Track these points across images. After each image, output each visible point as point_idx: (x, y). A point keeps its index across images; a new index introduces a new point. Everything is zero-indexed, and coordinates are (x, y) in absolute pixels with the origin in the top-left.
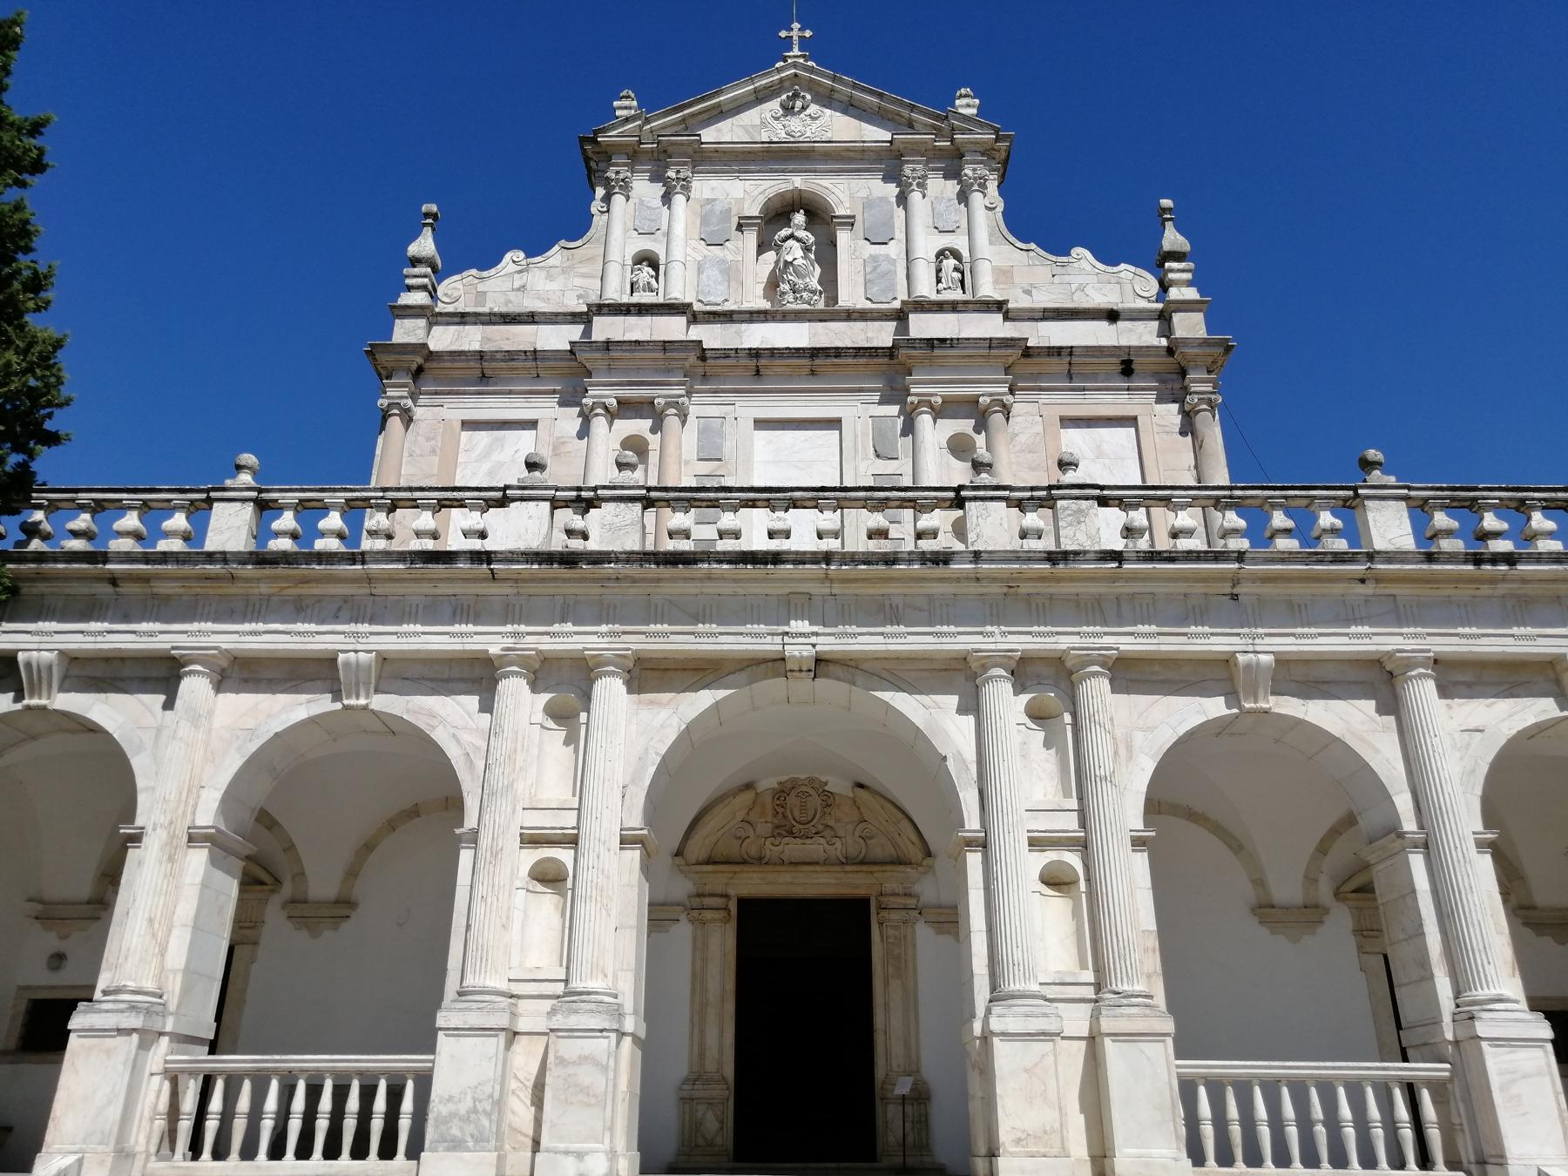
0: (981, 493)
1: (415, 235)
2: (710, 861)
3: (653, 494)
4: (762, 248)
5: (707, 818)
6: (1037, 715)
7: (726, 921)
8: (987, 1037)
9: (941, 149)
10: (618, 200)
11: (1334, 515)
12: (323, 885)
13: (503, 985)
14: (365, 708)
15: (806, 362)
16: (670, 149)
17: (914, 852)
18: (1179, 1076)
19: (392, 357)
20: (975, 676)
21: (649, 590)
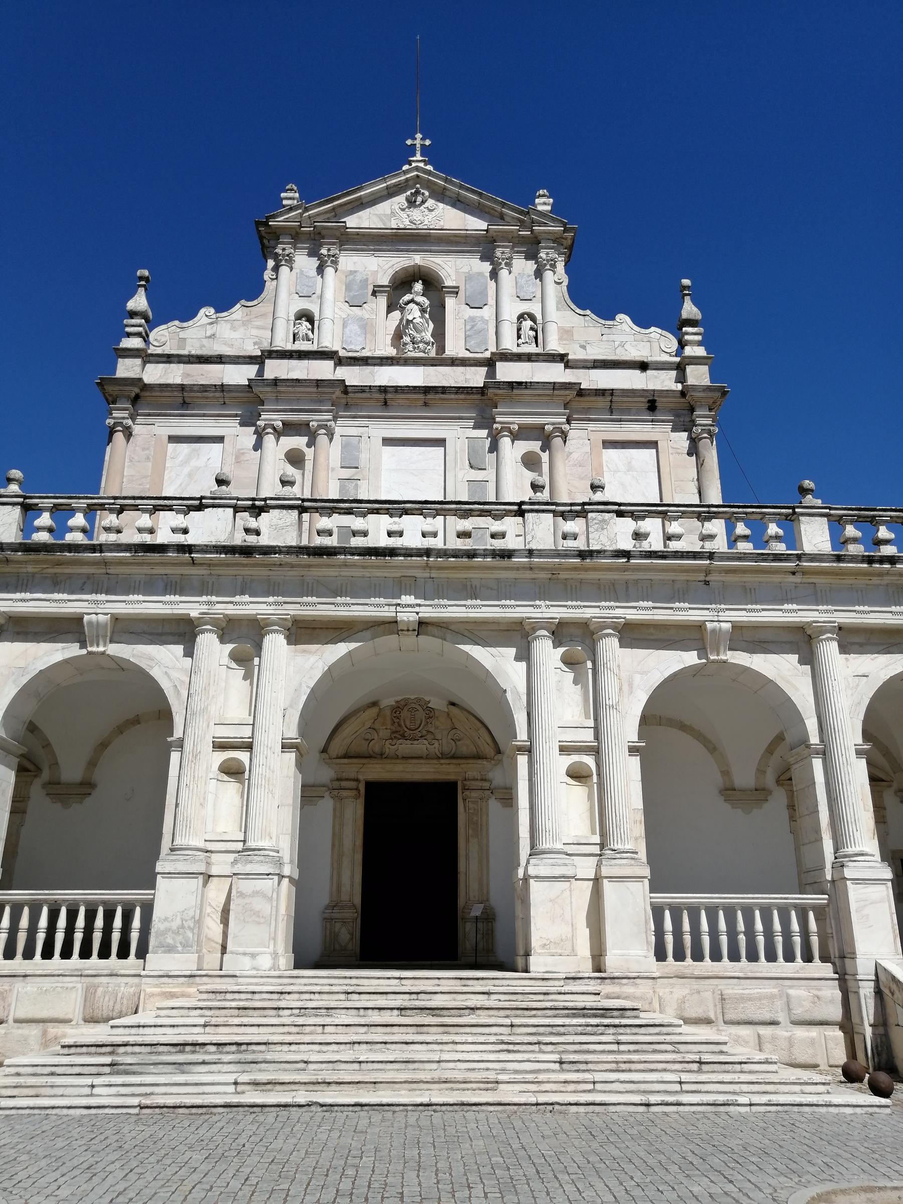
0: (536, 507)
1: (132, 295)
2: (346, 756)
3: (306, 504)
4: (390, 308)
5: (345, 726)
6: (569, 662)
7: (357, 797)
8: (526, 879)
9: (523, 237)
10: (284, 270)
11: (779, 526)
12: (71, 770)
13: (201, 844)
14: (103, 653)
15: (421, 396)
16: (324, 232)
17: (489, 751)
18: (651, 904)
19: (117, 388)
20: (527, 635)
21: (303, 573)
